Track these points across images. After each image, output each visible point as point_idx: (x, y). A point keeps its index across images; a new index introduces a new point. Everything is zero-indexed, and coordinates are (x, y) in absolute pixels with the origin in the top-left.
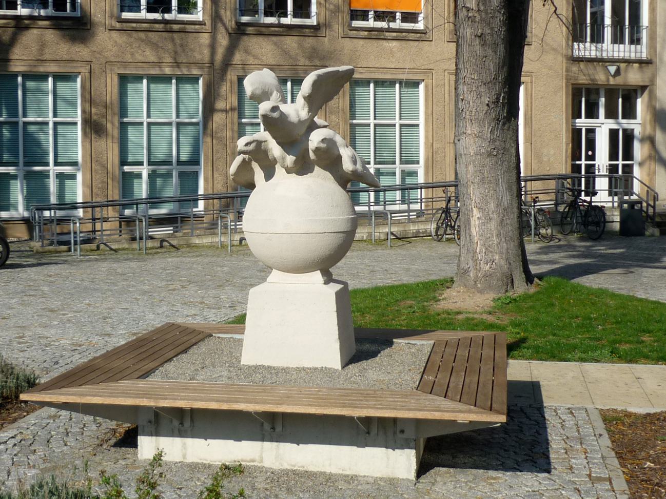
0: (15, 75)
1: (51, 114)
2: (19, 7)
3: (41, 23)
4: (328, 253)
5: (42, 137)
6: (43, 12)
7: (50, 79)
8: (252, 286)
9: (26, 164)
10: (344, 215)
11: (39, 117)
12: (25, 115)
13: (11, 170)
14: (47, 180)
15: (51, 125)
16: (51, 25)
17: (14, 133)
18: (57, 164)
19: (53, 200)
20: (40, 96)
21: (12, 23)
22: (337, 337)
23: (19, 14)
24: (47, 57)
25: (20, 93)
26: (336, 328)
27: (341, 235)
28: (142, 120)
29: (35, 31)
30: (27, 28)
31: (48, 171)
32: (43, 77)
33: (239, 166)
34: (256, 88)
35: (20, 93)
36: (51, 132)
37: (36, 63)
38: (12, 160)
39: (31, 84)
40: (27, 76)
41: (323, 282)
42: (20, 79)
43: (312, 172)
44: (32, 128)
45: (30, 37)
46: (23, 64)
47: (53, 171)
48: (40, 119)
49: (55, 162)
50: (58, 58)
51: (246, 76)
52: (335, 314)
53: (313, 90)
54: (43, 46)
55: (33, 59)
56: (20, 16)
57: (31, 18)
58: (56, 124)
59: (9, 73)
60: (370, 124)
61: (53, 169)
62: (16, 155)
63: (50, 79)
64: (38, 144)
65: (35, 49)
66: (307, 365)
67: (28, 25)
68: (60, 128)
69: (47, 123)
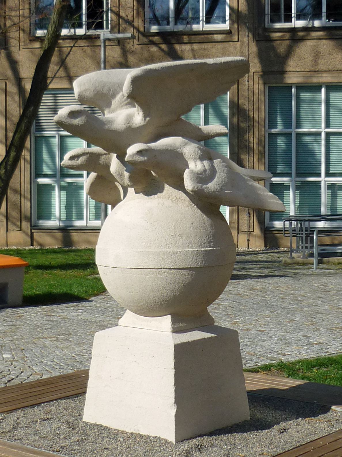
0: (290, 87)
1: (323, 125)
2: (293, 19)
3: (314, 34)
4: (170, 294)
5: (316, 146)
6: (317, 23)
7: (323, 90)
8: (103, 327)
9: (299, 174)
10: (192, 247)
11: (314, 127)
12: (298, 126)
13: (285, 180)
14: (81, 191)
15: (323, 136)
16: (326, 36)
17: (289, 145)
18: (328, 174)
19: (324, 210)
20: (315, 107)
21: (288, 35)
22: (173, 400)
23: (293, 26)
24: (321, 67)
25: (294, 103)
26: (172, 389)
27: (186, 272)
28: (320, 130)
29: (309, 43)
30: (302, 39)
31: (83, 182)
32: (317, 88)
33: (91, 184)
34: (86, 90)
35: (294, 103)
36: (323, 142)
37: (309, 74)
38: (287, 170)
39: (305, 95)
40: (300, 88)
41: (170, 330)
42: (294, 90)
43: (161, 191)
44: (308, 139)
45: (305, 49)
46: (296, 75)
47: (325, 182)
48: (314, 130)
49: (326, 173)
50: (330, 68)
51: (78, 77)
52: (173, 372)
53: (133, 89)
54: (317, 55)
55: (307, 70)
56: (295, 28)
57: (305, 29)
58: (328, 135)
59: (286, 85)
60: (321, 133)
61: (324, 180)
62: (288, 163)
63: (323, 90)
64: (312, 155)
65: (309, 58)
66: (143, 432)
67: (303, 36)
68: (332, 139)
69: (319, 134)
